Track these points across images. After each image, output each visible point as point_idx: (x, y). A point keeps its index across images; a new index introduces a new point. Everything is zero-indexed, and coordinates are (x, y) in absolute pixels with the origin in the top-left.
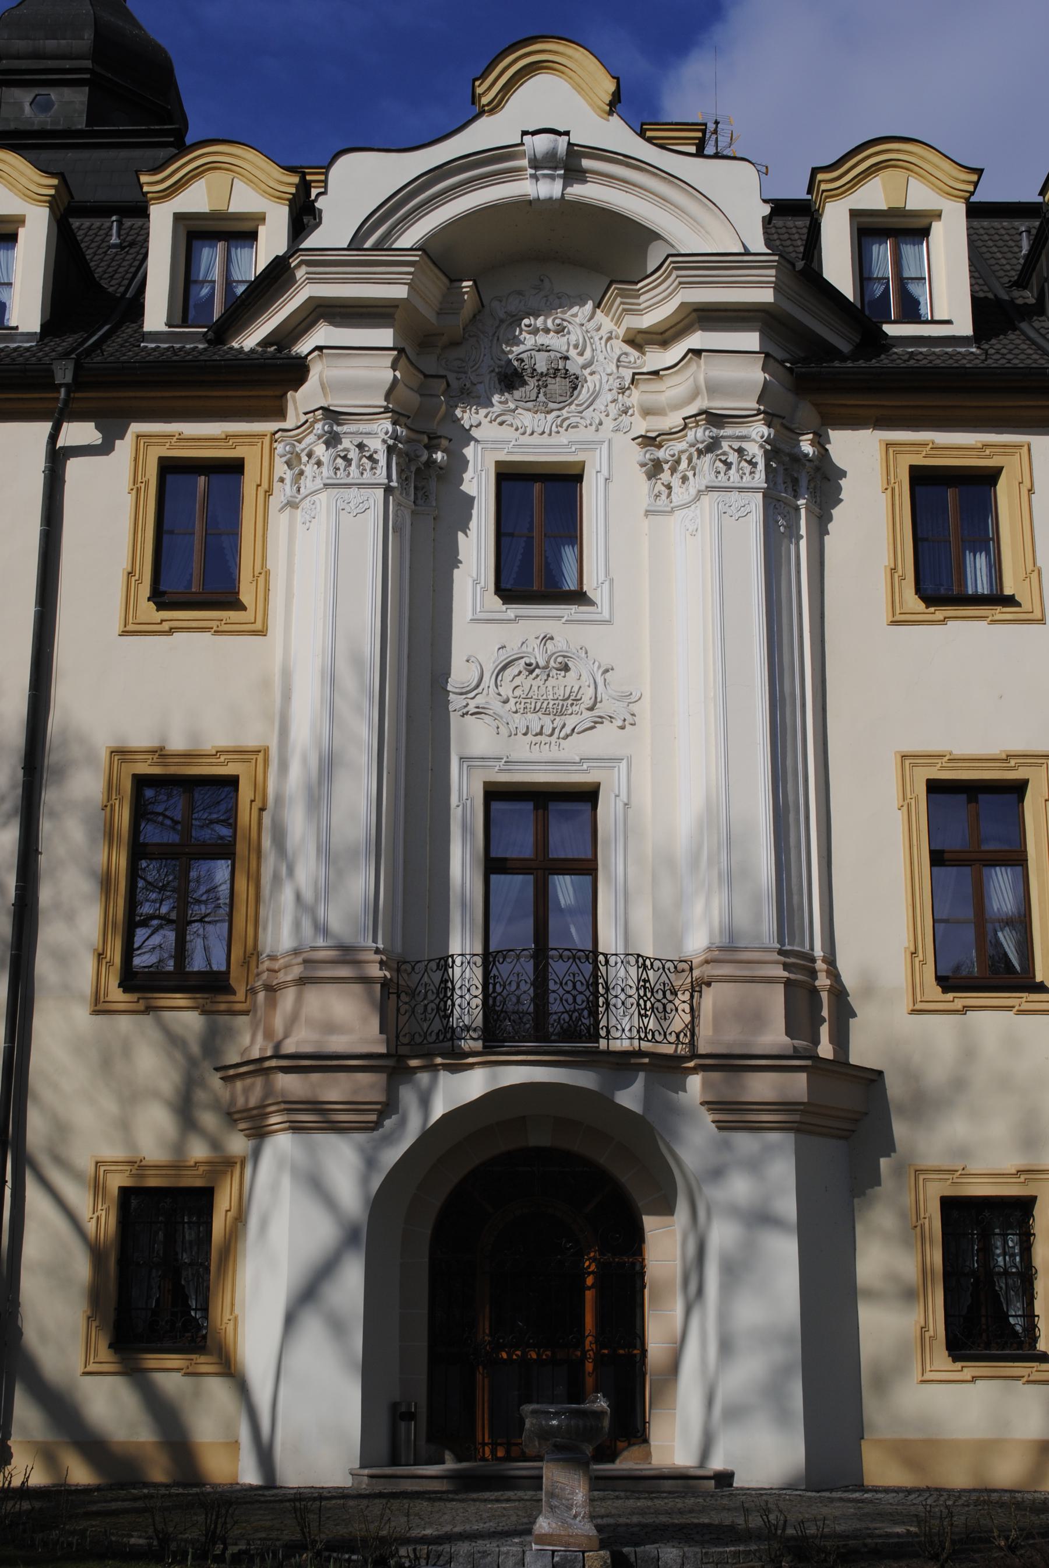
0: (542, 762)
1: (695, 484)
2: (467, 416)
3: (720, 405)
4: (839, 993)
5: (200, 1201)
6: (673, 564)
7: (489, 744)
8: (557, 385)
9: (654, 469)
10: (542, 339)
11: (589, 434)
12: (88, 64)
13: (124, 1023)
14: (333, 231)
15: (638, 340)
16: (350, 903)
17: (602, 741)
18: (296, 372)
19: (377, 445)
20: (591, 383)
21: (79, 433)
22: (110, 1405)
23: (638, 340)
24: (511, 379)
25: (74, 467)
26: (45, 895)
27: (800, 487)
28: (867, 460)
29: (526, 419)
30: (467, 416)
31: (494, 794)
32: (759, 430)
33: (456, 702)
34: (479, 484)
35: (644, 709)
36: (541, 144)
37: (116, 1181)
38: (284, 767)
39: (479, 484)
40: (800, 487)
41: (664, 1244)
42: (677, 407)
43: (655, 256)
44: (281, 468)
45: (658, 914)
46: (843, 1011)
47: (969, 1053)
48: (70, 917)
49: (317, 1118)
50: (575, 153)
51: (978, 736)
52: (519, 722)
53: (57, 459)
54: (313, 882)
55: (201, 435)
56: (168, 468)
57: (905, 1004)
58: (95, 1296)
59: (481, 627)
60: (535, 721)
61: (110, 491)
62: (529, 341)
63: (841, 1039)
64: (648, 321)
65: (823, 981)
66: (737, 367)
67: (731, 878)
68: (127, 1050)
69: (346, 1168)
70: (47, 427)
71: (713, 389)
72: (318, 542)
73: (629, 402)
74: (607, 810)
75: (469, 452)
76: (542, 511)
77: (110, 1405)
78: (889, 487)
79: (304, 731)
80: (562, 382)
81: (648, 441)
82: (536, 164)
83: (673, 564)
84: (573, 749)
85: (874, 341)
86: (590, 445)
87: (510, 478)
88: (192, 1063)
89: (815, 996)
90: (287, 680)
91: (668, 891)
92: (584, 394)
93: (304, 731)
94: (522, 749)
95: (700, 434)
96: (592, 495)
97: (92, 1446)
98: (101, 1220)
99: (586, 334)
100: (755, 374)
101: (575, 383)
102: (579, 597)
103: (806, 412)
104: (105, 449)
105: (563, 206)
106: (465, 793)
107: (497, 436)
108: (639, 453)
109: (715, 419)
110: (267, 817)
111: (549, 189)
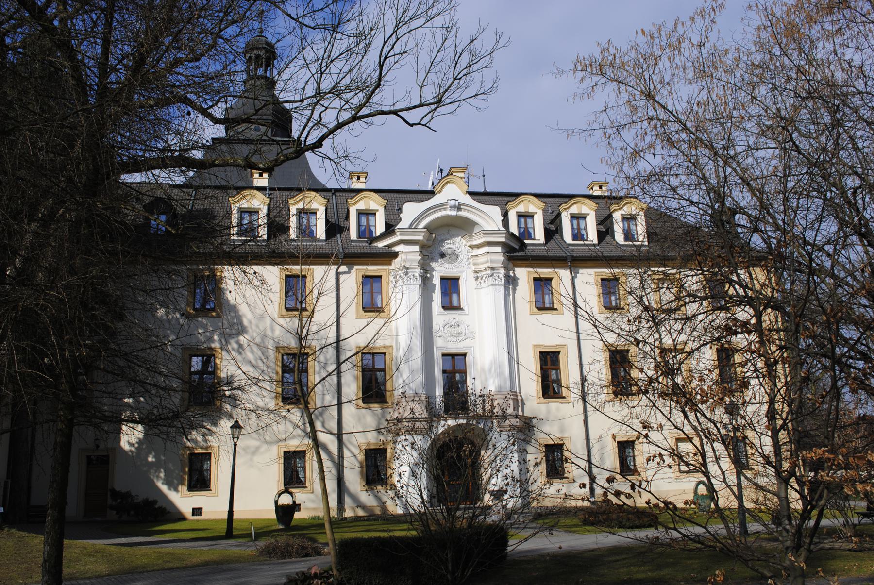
0: (454, 348)
1: (487, 284)
2: (433, 264)
3: (494, 265)
4: (522, 400)
5: (383, 451)
6: (482, 299)
7: (443, 344)
8: (453, 257)
9: (477, 278)
10: (449, 246)
11: (461, 269)
12: (270, 117)
13: (364, 411)
14: (404, 224)
15: (471, 247)
16: (417, 382)
17: (468, 342)
18: (395, 255)
19: (417, 275)
20: (461, 257)
21: (343, 268)
22: (367, 498)
23: (471, 247)
24: (443, 256)
25: (342, 278)
26: (343, 381)
27: (511, 282)
28: (524, 275)
29: (447, 265)
30: (433, 264)
31: (444, 355)
32: (502, 272)
33: (435, 334)
34: (437, 281)
35: (477, 335)
36: (452, 203)
37: (364, 447)
38: (398, 350)
39: (437, 281)
40: (511, 282)
41: (486, 455)
42: (483, 263)
43: (476, 230)
44: (392, 278)
45: (482, 383)
46: (523, 404)
47: (549, 412)
48: (349, 386)
49: (413, 431)
50: (460, 204)
51: (550, 342)
52: (449, 338)
53: (338, 274)
54: (407, 379)
55: (372, 269)
56: (366, 277)
57: (536, 402)
58: (361, 473)
59: (439, 317)
60: (452, 338)
61: (351, 281)
62: (447, 246)
63: (523, 410)
64: (476, 242)
65: (519, 398)
66: (497, 255)
67: (501, 374)
68: (364, 417)
69: (423, 443)
70: (336, 267)
71: (492, 261)
72: (403, 296)
73: (473, 261)
74: (468, 359)
75: (434, 273)
76: (451, 285)
77: (367, 498)
78: (529, 282)
79: (403, 341)
80: (455, 256)
81: (476, 272)
82: (451, 207)
83: (482, 299)
84: (461, 345)
85: (523, 246)
86: (462, 272)
87: (443, 279)
88: (380, 419)
89: (518, 402)
90: (398, 331)
91: (484, 378)
92: (460, 259)
93: (403, 341)
94: (450, 345)
95: (489, 272)
96: (462, 283)
97: (364, 507)
98: (361, 457)
99: (458, 244)
100: (501, 258)
101: (457, 257)
102: (459, 308)
103: (511, 265)
104: (349, 272)
105: (457, 217)
106: (437, 354)
107: (440, 269)
108: (473, 275)
109: (493, 269)
110: (394, 362)
111: (453, 213)
